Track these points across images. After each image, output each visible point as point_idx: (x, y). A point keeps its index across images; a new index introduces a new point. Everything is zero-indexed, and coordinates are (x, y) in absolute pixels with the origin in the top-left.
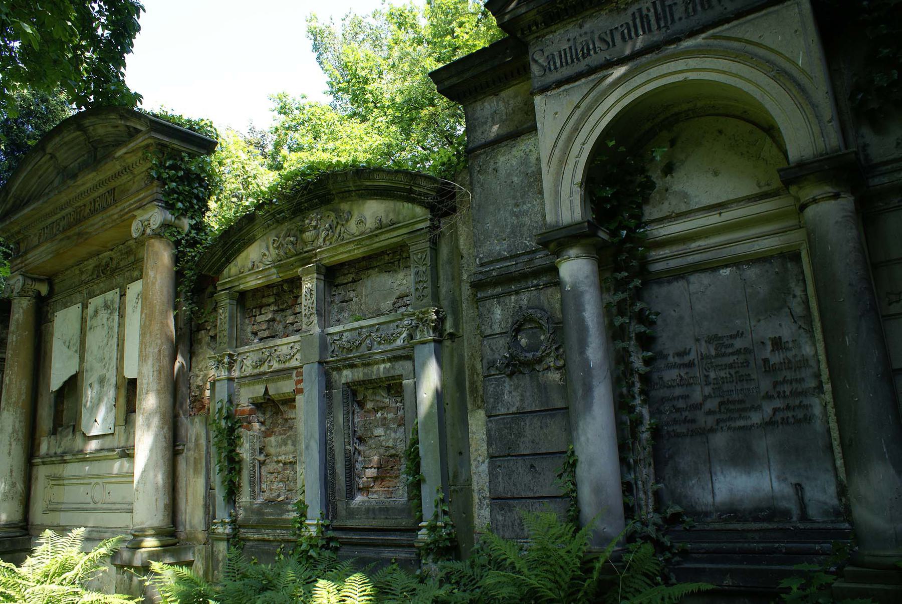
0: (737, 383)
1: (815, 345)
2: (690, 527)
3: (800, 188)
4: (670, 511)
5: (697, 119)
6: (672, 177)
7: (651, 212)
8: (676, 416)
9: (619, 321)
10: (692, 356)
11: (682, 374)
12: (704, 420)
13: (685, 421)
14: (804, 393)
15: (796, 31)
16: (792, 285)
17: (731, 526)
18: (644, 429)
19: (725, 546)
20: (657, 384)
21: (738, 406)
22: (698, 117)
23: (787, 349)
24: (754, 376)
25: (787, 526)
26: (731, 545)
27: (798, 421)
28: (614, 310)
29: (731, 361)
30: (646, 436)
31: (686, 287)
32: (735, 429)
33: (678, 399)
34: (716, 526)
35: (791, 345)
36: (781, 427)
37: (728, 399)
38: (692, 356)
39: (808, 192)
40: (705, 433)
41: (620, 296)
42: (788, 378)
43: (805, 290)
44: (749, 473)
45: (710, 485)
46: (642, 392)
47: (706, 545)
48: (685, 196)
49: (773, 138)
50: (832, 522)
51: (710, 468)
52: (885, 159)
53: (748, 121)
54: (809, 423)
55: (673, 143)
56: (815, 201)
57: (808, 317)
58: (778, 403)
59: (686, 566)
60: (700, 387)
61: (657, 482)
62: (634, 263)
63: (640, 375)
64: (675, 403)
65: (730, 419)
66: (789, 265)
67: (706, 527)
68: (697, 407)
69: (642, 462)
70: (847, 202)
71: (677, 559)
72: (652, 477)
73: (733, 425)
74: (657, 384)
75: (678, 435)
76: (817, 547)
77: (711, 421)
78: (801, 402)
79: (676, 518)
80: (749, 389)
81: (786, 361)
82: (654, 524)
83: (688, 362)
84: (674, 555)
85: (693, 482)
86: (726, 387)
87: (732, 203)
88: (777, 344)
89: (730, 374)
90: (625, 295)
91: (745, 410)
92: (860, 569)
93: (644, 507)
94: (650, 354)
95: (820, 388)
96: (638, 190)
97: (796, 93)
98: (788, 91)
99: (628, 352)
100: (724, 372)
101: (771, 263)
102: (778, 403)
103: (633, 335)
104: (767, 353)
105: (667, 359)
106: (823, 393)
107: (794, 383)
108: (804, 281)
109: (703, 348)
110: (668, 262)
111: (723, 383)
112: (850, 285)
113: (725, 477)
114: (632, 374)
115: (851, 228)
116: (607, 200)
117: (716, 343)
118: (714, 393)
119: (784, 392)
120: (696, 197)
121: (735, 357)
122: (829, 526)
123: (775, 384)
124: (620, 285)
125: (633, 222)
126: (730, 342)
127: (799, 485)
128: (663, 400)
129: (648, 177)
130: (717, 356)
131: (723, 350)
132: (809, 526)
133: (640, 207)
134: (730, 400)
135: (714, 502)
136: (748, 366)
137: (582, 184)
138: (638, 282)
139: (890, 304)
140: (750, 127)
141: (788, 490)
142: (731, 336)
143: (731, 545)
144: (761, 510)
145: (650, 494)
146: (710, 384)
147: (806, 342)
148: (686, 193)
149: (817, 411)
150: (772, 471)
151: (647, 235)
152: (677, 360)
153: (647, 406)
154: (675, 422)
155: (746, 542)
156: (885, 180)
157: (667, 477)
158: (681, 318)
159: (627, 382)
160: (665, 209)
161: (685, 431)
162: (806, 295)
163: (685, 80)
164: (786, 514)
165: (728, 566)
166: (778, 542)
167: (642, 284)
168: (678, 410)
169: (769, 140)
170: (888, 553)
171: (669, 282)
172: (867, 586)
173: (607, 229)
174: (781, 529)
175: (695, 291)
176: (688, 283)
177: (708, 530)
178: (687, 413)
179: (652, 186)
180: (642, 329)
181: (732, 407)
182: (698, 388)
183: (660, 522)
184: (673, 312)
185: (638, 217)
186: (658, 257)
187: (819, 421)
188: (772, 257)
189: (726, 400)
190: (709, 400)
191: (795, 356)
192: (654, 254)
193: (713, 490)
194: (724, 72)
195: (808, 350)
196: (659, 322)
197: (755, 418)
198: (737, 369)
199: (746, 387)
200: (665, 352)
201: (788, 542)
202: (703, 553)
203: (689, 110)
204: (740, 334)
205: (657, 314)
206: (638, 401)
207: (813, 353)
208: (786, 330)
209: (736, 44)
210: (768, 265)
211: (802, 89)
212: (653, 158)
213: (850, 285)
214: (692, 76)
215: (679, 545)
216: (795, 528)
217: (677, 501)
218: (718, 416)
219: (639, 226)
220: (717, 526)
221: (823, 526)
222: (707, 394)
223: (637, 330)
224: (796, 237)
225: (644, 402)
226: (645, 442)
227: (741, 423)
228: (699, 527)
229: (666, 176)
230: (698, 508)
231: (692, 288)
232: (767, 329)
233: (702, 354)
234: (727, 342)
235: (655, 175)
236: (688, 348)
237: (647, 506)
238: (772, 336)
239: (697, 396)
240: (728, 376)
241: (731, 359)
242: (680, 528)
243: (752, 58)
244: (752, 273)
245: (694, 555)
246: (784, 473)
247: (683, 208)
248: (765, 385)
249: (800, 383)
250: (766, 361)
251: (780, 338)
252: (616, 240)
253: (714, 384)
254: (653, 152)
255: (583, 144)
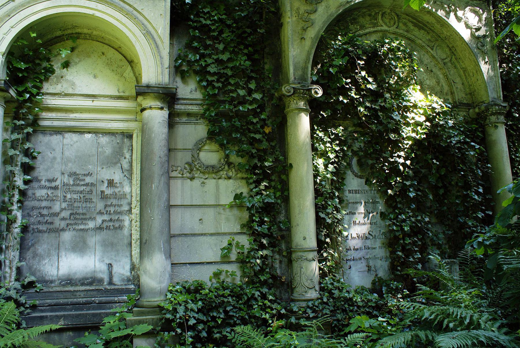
0: (83, 203)
1: (131, 187)
2: (40, 290)
3: (144, 99)
4: (27, 280)
5: (91, 41)
6: (67, 70)
7: (47, 87)
8: (41, 219)
9: (11, 152)
10: (58, 183)
11: (49, 193)
12: (58, 223)
13: (46, 223)
14: (120, 213)
15: (161, 15)
16: (125, 151)
17: (67, 289)
18: (16, 226)
19: (61, 301)
20: (30, 197)
21: (82, 217)
22: (92, 40)
23: (116, 187)
24: (94, 200)
25: (101, 288)
26: (66, 300)
27: (115, 228)
28: (9, 145)
29: (82, 189)
30: (18, 230)
31: (62, 139)
32: (78, 230)
33: (44, 209)
34: (57, 289)
35: (118, 185)
36: (105, 230)
37: (76, 212)
38: (58, 183)
39: (147, 102)
40: (58, 231)
41: (15, 136)
42: (114, 203)
43: (132, 156)
44: (83, 257)
45: (57, 264)
46: (19, 201)
47: (49, 301)
48: (73, 84)
49: (132, 67)
50: (125, 285)
51: (58, 253)
52: (184, 97)
53: (120, 53)
54: (121, 230)
55: (73, 50)
56: (151, 108)
57: (130, 171)
58: (106, 217)
59: (34, 315)
60: (59, 202)
61: (20, 261)
62: (30, 117)
63: (20, 191)
64: (42, 211)
65: (76, 224)
66: (125, 140)
67: (51, 290)
68: (56, 215)
69: (12, 248)
70: (165, 113)
71: (29, 311)
72: (17, 257)
73: (77, 227)
74: (30, 197)
75: (40, 231)
76: (116, 299)
77: (63, 224)
78: (118, 218)
79: (31, 284)
80: (90, 207)
81: (114, 194)
82: (15, 289)
83: (54, 186)
84: (27, 308)
85: (46, 261)
86: (76, 205)
87: (101, 97)
88: (111, 183)
89: (80, 197)
90: (20, 136)
91: (85, 219)
92: (142, 309)
93: (8, 279)
94: (29, 177)
95: (130, 211)
96: (43, 71)
97: (154, 47)
98: (150, 45)
99: (14, 173)
100: (77, 195)
101: (116, 137)
102: (106, 217)
103: (19, 164)
104: (104, 187)
105: (40, 182)
106: (131, 214)
107: (116, 207)
108: (132, 150)
109: (66, 179)
110: (53, 122)
111: (75, 202)
112: (160, 157)
113: (67, 259)
114: (13, 189)
115: (166, 128)
116: (20, 70)
117: (74, 177)
118: (68, 207)
119: (110, 211)
120: (80, 87)
121: (85, 188)
122: (124, 287)
123: (106, 206)
124: (16, 129)
125: (34, 91)
126: (83, 178)
127: (111, 264)
128: (33, 208)
129: (52, 66)
130: (74, 185)
131: (78, 182)
132: (113, 287)
133: (41, 82)
134: (78, 212)
135: (58, 274)
136: (91, 194)
137: (4, 54)
138: (30, 130)
139: (172, 171)
140: (121, 57)
141: (104, 267)
142: (84, 174)
143: (66, 300)
144: (87, 279)
145: (14, 269)
146: (66, 201)
147: (127, 185)
148: (74, 83)
149: (127, 223)
150: (96, 256)
151: (43, 101)
152: (48, 184)
153: (21, 211)
154: (39, 223)
155: (75, 298)
156: (183, 107)
157: (28, 258)
158: (55, 158)
159: (9, 194)
160: (58, 89)
161: (45, 229)
162: (132, 158)
163: (93, 15)
164: (100, 281)
165: (62, 313)
166: (94, 297)
167: (33, 131)
168: (42, 215)
169: (129, 68)
170: (156, 300)
171: (51, 135)
172: (144, 317)
173: (16, 90)
174: (97, 290)
175: (66, 143)
176: (64, 138)
177: (52, 292)
178: (48, 218)
179: (53, 72)
180: (27, 160)
181: (78, 217)
182: (59, 203)
183: (19, 287)
184: (50, 154)
185: (39, 88)
186: (47, 117)
187: (127, 229)
188: (117, 133)
189: (75, 212)
190: (64, 211)
191: (119, 192)
192: (44, 115)
193: (58, 267)
194: (117, 20)
195: (127, 189)
196: (39, 158)
197: (91, 225)
198: (85, 195)
199: (89, 206)
200: (40, 178)
201: (100, 297)
202: (47, 306)
203: (87, 34)
204: (89, 174)
205: (39, 153)
206: (15, 207)
207: (129, 191)
208: (117, 176)
209: (127, 7)
210: (114, 137)
211: (157, 47)
212: (59, 54)
213: (160, 157)
214: (98, 14)
215: (30, 302)
216: (105, 289)
217: (33, 274)
218: (68, 222)
219: (38, 94)
220: (58, 289)
221: (120, 287)
222: (63, 208)
223: (23, 161)
224: (131, 126)
225: (20, 208)
226: (15, 235)
227: (82, 227)
228: (45, 289)
229: (64, 69)
230: (47, 278)
231: (65, 141)
232: (106, 174)
233: (64, 182)
234: (81, 178)
235: (57, 66)
236: (56, 177)
237: (10, 277)
238: (109, 179)
239: (57, 208)
240: (79, 198)
241: (82, 188)
242: (32, 290)
243: (135, 19)
244: (104, 140)
245: (39, 308)
246: (103, 258)
247: (70, 91)
248: (100, 206)
249: (120, 207)
250: (102, 192)
251: (113, 180)
252: (21, 99)
253: (69, 202)
254: (60, 50)
255: (12, 28)
